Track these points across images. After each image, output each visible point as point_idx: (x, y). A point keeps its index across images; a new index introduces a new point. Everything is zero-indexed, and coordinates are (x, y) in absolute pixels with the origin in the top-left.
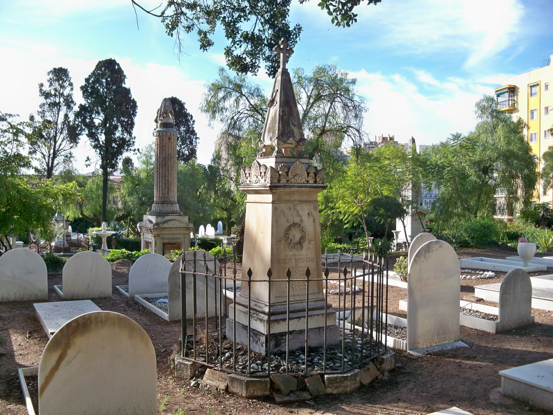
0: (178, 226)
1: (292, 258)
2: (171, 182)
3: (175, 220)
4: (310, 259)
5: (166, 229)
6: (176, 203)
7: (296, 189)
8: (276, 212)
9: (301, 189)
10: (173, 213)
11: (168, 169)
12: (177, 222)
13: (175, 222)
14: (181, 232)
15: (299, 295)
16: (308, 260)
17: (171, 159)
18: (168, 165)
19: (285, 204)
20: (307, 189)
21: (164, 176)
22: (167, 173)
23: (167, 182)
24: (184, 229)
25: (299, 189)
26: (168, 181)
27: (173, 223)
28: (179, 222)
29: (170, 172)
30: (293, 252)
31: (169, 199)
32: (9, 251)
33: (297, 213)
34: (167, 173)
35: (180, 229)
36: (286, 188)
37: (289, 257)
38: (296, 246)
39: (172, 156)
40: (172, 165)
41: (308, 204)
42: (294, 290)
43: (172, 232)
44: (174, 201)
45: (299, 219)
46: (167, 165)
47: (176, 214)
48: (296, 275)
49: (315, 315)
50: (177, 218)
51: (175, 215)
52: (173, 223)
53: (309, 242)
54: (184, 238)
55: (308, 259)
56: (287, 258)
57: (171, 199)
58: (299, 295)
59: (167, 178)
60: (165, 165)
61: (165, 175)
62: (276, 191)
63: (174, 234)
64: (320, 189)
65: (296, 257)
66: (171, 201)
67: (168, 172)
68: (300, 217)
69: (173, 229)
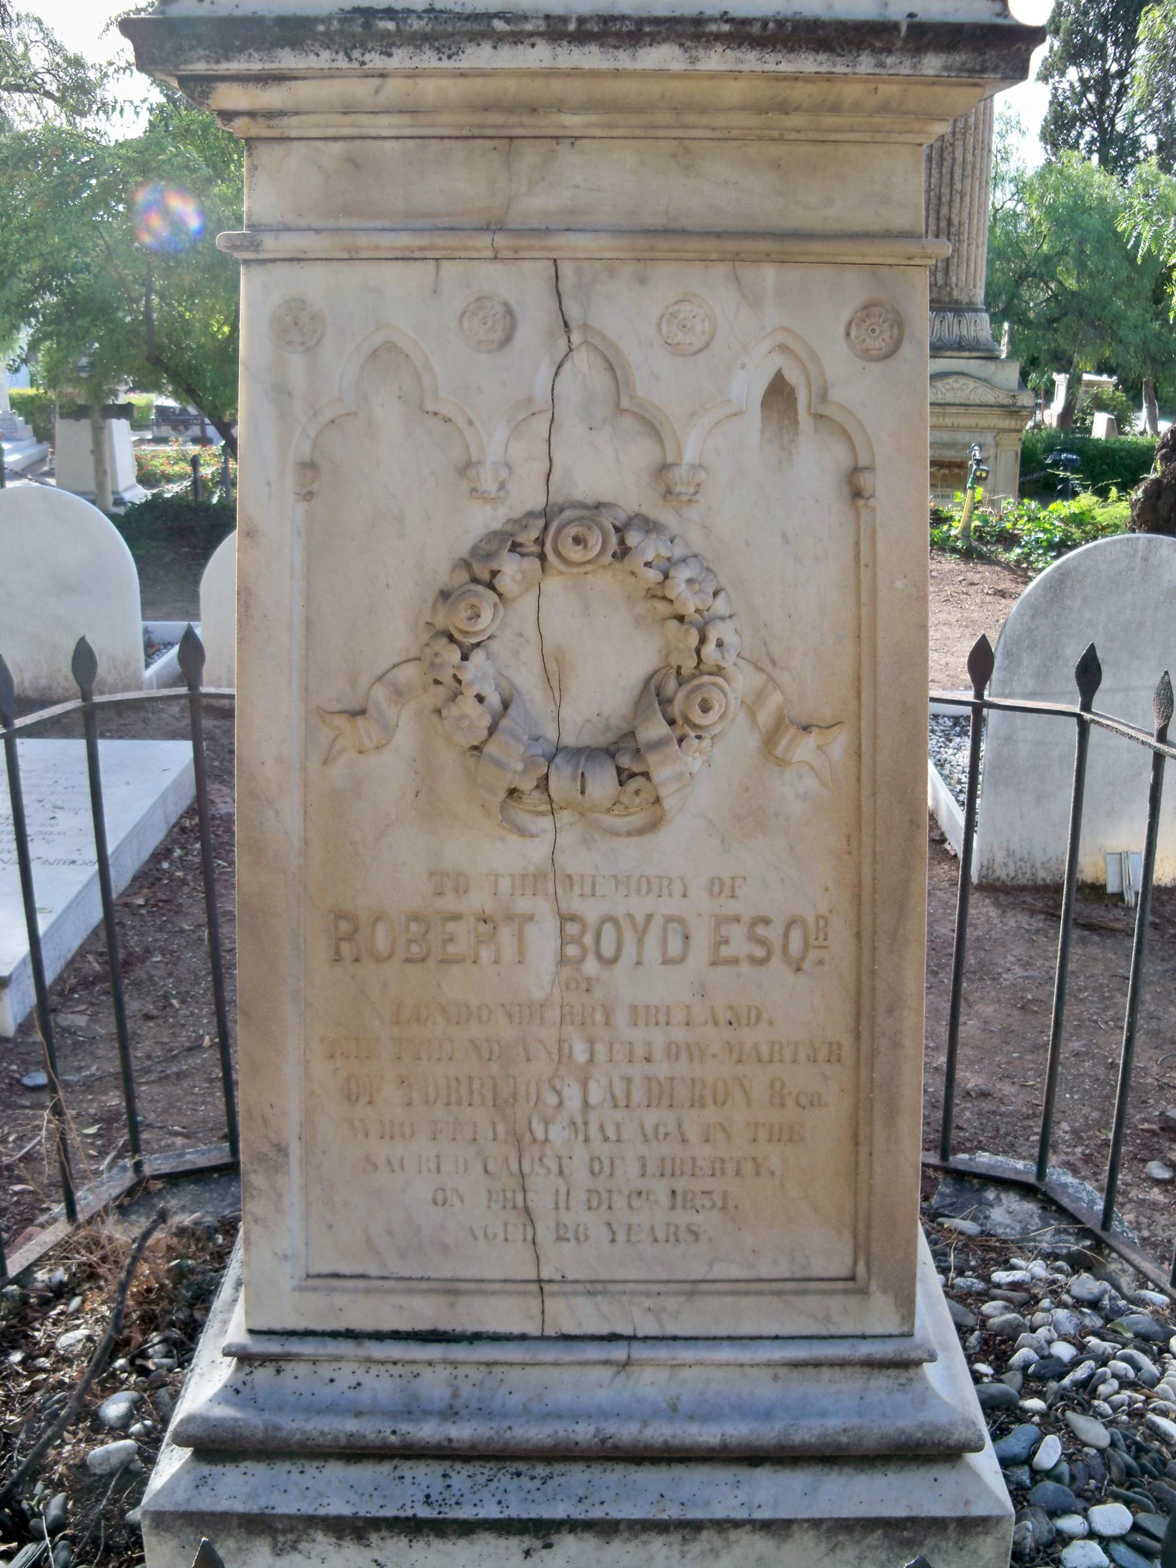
0: (975, 399)
1: (523, 905)
2: (960, 224)
3: (963, 374)
4: (773, 934)
5: (949, 410)
6: (976, 310)
7: (539, 55)
8: (297, 362)
9: (623, 59)
10: (961, 348)
11: (952, 173)
12: (971, 384)
13: (963, 380)
14: (983, 423)
15: (596, 1288)
16: (738, 945)
17: (964, 134)
18: (954, 159)
19: (421, 273)
20: (715, 60)
21: (934, 201)
22: (946, 191)
23: (943, 224)
24: (998, 411)
25: (591, 58)
26: (949, 222)
27: (956, 386)
28: (978, 384)
29: (958, 186)
30: (536, 852)
31: (950, 294)
32: (929, 420)
33: (601, 380)
34: (946, 191)
35: (982, 410)
36: (387, 45)
37: (478, 900)
38: (561, 782)
39: (972, 121)
40: (969, 157)
41: (769, 274)
42: (545, 1232)
43: (948, 421)
44: (971, 303)
45: (642, 454)
46: (948, 158)
47: (970, 350)
48: (572, 1093)
49: (737, 1524)
50: (973, 366)
51: (967, 354)
52: (956, 386)
53: (770, 740)
54: (997, 445)
55: (736, 933)
56: (450, 903)
57: (956, 293)
58: (596, 1288)
59: (944, 211)
60: (942, 158)
61: (940, 198)
62: (271, 97)
63: (955, 428)
64: (932, 63)
65: (575, 904)
66: (957, 302)
67: (952, 184)
68: (652, 427)
69: (954, 410)
